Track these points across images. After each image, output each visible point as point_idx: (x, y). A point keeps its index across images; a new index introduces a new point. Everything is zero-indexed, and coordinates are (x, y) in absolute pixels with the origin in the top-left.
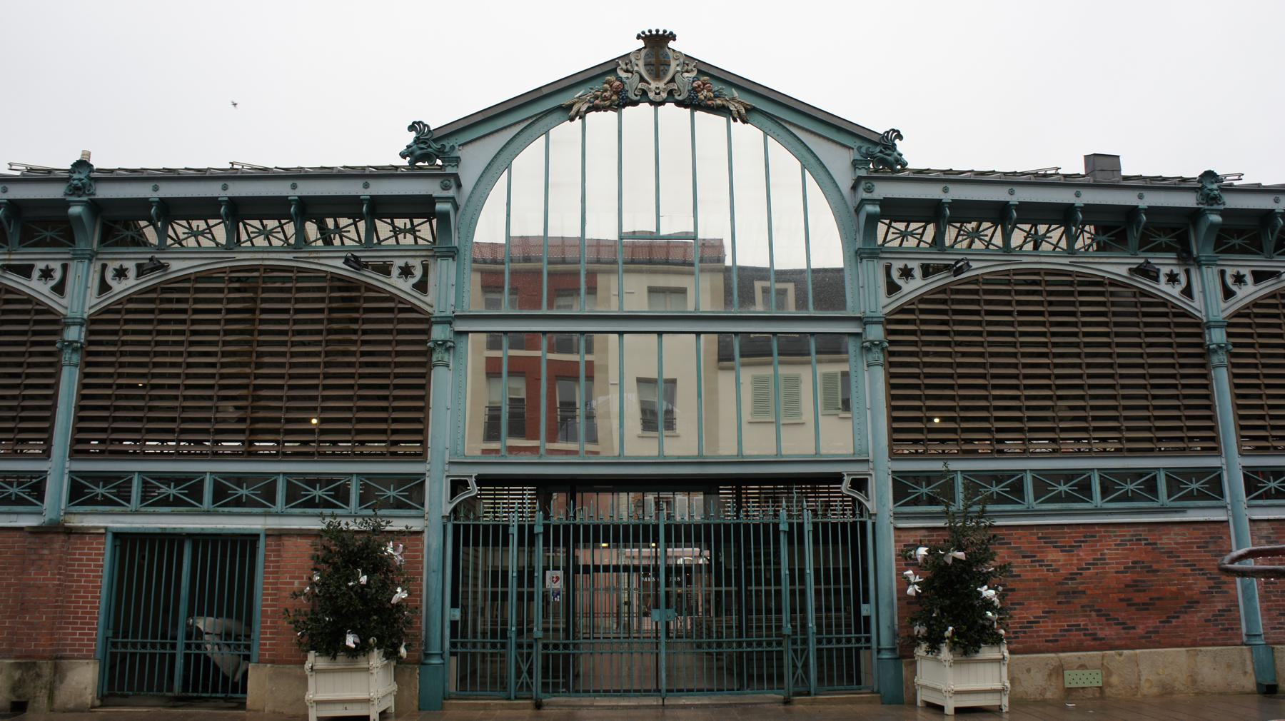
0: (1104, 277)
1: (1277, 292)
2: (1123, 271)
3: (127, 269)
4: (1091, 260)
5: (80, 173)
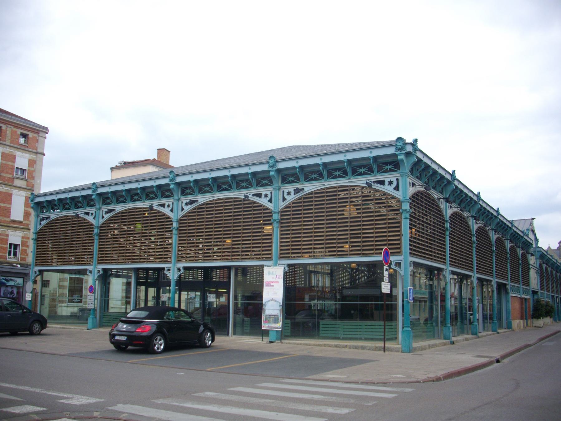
3: (393, 181)
5: (399, 142)
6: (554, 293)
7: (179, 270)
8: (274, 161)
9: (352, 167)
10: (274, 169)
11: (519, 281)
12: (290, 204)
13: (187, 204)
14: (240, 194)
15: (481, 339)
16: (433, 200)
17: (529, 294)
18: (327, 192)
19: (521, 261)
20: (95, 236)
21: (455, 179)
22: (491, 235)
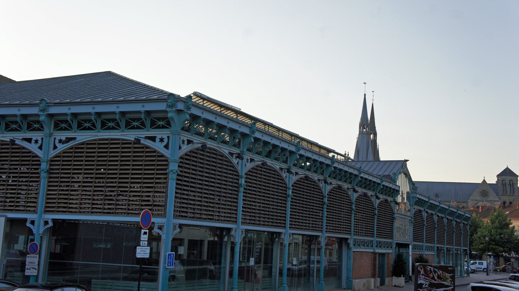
0: (224, 154)
3: (164, 138)
7: (46, 223)
8: (45, 105)
9: (78, 121)
10: (45, 113)
13: (60, 141)
14: (131, 135)
17: (434, 251)
18: (99, 144)
20: (43, 172)
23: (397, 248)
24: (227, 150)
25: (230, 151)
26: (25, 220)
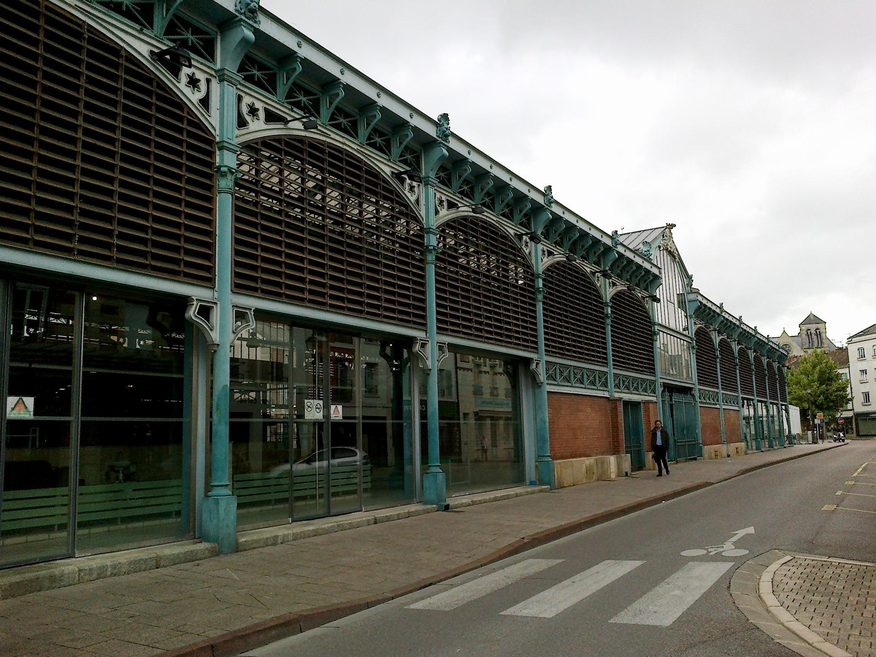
1: (282, 137)
2: (144, 49)
4: (373, 155)
6: (767, 398)
11: (606, 359)
12: (257, 143)
15: (252, 555)
16: (583, 275)
17: (737, 404)
19: (541, 281)
21: (551, 201)
22: (713, 337)
23: (667, 394)
24: (143, 44)
25: (267, 106)
26: (184, 301)
